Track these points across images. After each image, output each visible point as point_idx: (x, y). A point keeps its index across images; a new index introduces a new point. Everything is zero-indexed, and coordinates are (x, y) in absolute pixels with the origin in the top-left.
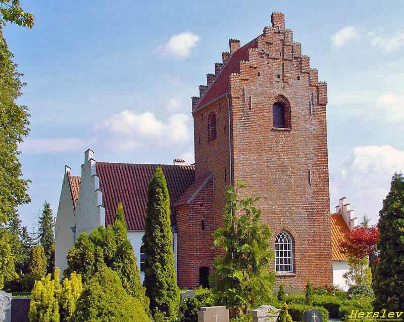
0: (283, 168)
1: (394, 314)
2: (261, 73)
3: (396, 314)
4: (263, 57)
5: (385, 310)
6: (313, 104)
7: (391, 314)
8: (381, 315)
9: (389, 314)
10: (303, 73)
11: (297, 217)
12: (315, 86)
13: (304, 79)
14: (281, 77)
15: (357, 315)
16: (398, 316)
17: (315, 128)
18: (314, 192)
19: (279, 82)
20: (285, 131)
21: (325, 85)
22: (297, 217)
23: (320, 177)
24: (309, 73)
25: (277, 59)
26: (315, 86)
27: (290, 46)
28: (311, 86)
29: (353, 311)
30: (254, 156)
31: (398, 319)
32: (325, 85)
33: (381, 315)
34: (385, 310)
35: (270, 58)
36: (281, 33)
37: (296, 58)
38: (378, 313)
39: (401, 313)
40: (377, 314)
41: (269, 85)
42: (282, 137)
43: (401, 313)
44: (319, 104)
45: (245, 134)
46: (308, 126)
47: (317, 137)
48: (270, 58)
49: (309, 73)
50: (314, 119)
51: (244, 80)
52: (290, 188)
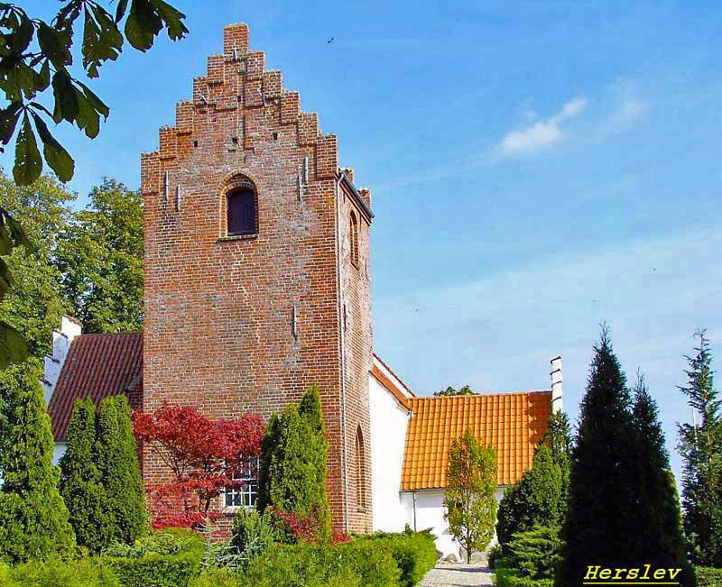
0: (238, 311)
1: (664, 573)
2: (200, 140)
3: (668, 573)
4: (205, 112)
5: (648, 566)
6: (304, 181)
7: (659, 573)
8: (641, 574)
9: (656, 573)
10: (285, 124)
11: (266, 400)
12: (310, 145)
13: (286, 138)
14: (240, 141)
15: (598, 575)
16: (672, 577)
17: (308, 225)
18: (304, 349)
19: (234, 151)
20: (244, 239)
21: (331, 140)
22: (266, 400)
23: (316, 320)
24: (296, 123)
25: (232, 110)
26: (310, 145)
27: (258, 80)
28: (301, 146)
29: (590, 567)
30: (184, 294)
31: (673, 581)
32: (331, 140)
33: (641, 574)
34: (648, 566)
35: (219, 111)
36: (239, 60)
37: (270, 100)
38: (637, 570)
39: (678, 570)
40: (631, 576)
41: (215, 159)
42: (240, 255)
43: (678, 570)
44: (317, 179)
45: (167, 256)
46: (294, 224)
47: (314, 243)
48: (219, 111)
49: (296, 123)
50: (307, 210)
51: (167, 159)
52: (253, 346)
